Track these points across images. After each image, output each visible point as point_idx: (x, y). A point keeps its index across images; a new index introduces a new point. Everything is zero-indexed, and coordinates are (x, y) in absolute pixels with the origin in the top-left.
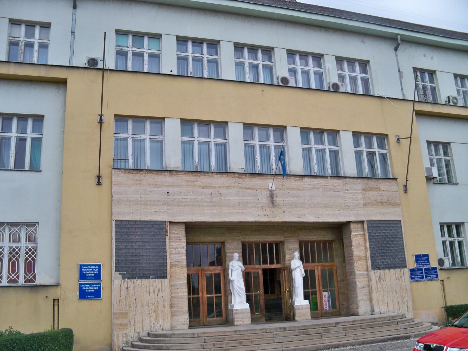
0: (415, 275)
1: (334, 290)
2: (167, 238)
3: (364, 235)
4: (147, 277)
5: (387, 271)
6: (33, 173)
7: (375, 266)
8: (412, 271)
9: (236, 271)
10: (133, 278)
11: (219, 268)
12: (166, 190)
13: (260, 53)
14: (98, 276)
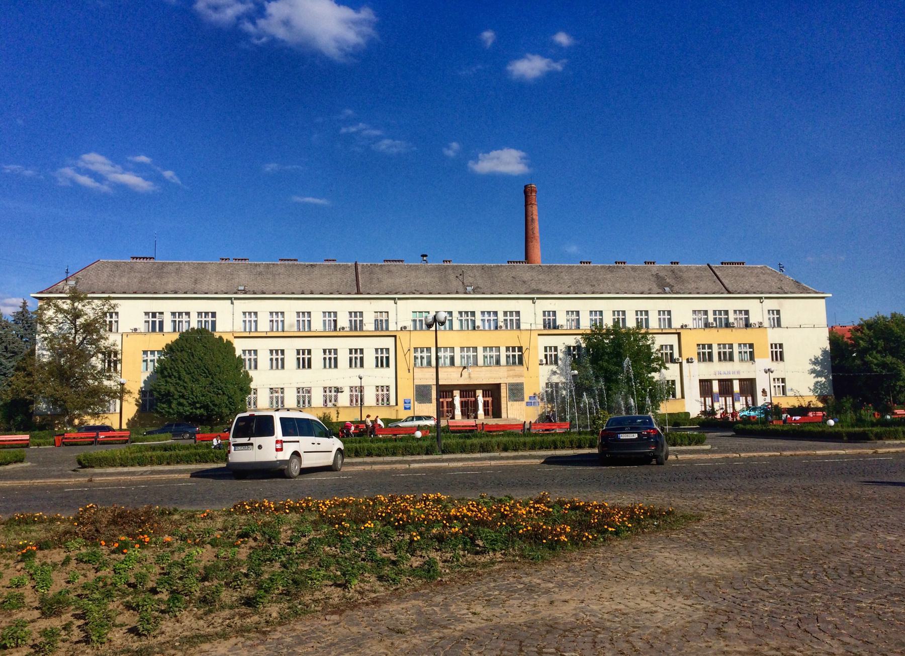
0: (528, 404)
9: (457, 401)
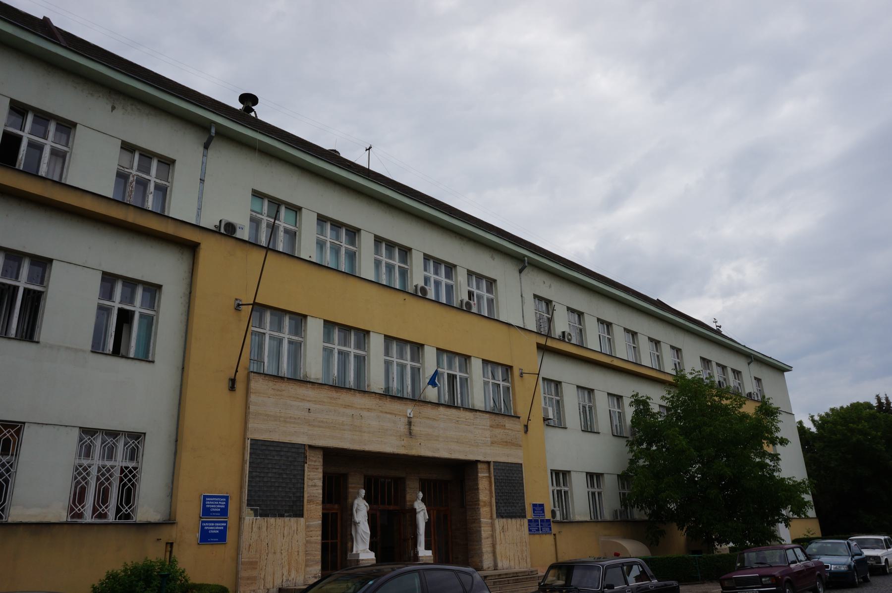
1: (456, 539)
2: (306, 465)
3: (490, 477)
4: (282, 516)
5: (509, 520)
6: (144, 365)
7: (500, 515)
8: (530, 521)
10: (267, 515)
11: (336, 506)
12: (308, 405)
13: (52, 127)
14: (224, 512)
